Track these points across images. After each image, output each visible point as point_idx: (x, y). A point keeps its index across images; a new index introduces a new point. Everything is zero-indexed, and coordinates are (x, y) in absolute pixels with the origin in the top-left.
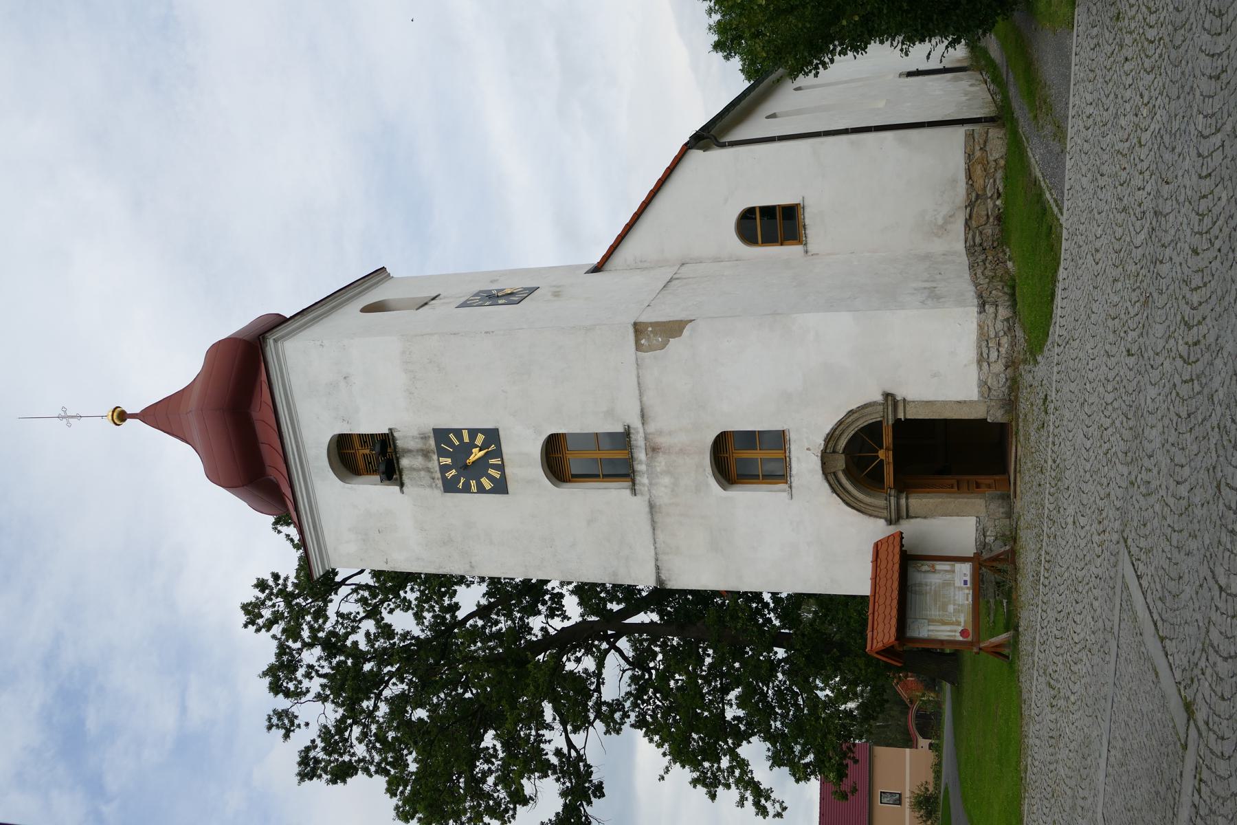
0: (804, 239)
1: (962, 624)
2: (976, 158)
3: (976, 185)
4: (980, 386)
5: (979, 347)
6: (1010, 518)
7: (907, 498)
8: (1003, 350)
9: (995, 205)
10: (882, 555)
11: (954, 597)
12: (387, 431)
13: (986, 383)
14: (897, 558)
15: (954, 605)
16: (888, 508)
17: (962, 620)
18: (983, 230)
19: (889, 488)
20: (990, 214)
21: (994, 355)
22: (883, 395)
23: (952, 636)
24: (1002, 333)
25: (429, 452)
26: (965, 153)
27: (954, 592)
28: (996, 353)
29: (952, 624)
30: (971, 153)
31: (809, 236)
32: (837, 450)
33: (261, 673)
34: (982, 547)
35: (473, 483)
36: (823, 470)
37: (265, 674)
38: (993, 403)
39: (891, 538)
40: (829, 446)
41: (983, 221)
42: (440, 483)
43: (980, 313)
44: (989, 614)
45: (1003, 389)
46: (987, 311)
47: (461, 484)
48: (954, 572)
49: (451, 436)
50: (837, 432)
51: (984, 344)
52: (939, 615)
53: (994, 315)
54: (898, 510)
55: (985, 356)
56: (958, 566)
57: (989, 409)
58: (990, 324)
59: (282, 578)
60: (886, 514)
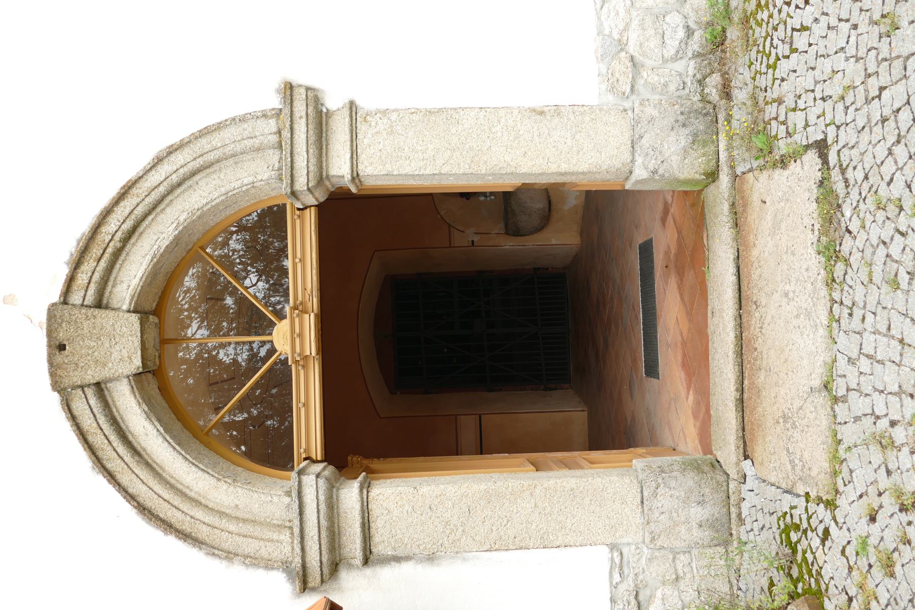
6: (726, 543)
7: (366, 487)
13: (622, 46)
32: (115, 303)
36: (52, 375)
40: (82, 278)
60: (287, 549)
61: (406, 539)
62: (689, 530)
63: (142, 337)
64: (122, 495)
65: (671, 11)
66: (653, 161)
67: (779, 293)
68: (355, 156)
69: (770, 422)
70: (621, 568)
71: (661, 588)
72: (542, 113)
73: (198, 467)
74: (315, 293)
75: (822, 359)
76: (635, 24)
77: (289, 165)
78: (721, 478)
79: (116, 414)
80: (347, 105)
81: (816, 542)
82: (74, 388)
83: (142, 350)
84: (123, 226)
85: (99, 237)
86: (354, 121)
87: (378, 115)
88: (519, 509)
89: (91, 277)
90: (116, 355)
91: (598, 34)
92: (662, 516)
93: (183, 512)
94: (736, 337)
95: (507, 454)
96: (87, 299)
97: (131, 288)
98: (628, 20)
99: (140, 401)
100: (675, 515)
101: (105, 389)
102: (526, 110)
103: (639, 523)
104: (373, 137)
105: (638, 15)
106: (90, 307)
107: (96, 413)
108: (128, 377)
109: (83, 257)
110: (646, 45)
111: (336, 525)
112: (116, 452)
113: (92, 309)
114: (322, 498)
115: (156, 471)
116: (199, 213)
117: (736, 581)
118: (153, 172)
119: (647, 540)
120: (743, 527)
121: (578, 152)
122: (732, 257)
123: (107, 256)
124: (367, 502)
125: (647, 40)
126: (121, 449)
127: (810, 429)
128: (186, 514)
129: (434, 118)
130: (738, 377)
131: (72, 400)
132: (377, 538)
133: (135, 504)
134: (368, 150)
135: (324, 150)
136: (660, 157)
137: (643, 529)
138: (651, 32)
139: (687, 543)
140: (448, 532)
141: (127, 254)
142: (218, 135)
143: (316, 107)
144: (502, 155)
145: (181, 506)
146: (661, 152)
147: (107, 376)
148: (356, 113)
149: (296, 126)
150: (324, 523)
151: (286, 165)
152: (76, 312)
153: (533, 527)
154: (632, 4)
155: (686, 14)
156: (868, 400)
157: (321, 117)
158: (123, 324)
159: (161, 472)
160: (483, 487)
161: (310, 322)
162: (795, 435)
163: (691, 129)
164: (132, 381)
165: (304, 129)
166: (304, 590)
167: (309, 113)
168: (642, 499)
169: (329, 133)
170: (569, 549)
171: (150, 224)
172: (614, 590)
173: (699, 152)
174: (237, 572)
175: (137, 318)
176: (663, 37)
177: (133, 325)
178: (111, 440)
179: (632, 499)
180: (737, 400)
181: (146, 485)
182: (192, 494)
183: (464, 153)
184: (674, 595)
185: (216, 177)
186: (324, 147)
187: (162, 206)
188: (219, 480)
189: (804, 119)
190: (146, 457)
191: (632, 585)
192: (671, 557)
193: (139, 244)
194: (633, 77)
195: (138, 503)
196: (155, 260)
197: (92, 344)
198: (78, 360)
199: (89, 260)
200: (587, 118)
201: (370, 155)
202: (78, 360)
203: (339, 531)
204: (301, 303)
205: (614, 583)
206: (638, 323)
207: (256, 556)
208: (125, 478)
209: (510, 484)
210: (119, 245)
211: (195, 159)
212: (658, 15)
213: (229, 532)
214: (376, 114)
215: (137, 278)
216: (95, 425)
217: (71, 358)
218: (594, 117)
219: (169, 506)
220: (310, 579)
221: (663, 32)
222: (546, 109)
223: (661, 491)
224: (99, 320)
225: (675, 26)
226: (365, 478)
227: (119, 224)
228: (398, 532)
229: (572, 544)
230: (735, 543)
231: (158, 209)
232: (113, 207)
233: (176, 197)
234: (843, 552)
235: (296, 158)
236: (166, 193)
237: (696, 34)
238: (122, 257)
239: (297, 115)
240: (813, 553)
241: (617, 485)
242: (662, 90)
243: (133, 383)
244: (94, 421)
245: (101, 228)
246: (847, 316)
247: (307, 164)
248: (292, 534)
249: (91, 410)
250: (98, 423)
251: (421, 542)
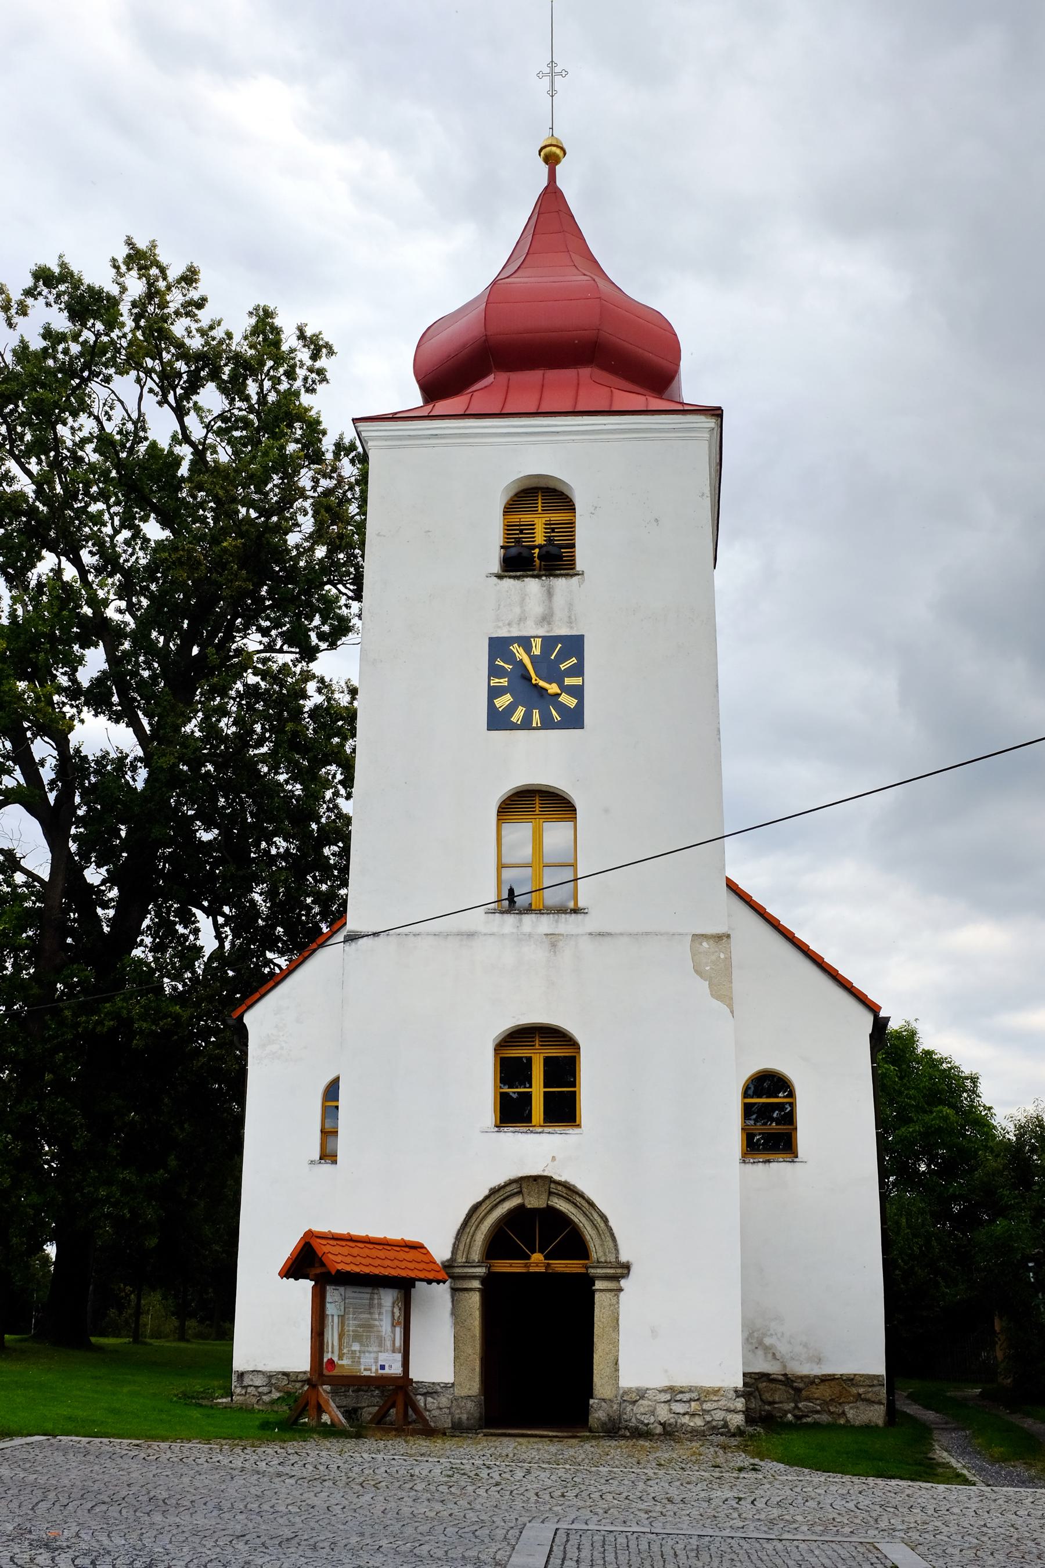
0: (752, 1161)
1: (340, 1362)
2: (848, 1388)
3: (813, 1389)
5: (691, 1390)
8: (686, 1420)
9: (786, 1412)
10: (412, 1254)
11: (368, 1352)
12: (579, 567)
13: (642, 1397)
14: (412, 1274)
15: (360, 1352)
16: (469, 1263)
17: (345, 1362)
18: (755, 1397)
19: (490, 1266)
20: (776, 1406)
21: (679, 1408)
22: (628, 1262)
23: (328, 1348)
24: (708, 1418)
25: (549, 623)
26: (855, 1375)
27: (375, 1352)
28: (682, 1411)
29: (340, 1349)
30: (854, 1382)
31: (755, 1166)
33: (66, 261)
35: (504, 682)
37: (63, 265)
40: (560, 1188)
41: (767, 1396)
42: (503, 633)
43: (736, 1391)
45: (633, 1420)
46: (737, 1400)
47: (502, 664)
48: (394, 1352)
49: (574, 660)
50: (578, 1199)
51: (694, 1395)
52: (348, 1331)
53: (733, 1408)
55: (679, 1397)
56: (399, 1357)
57: (608, 1402)
58: (720, 1403)
59: (196, 311)
60: (460, 1260)
76: (650, 1403)
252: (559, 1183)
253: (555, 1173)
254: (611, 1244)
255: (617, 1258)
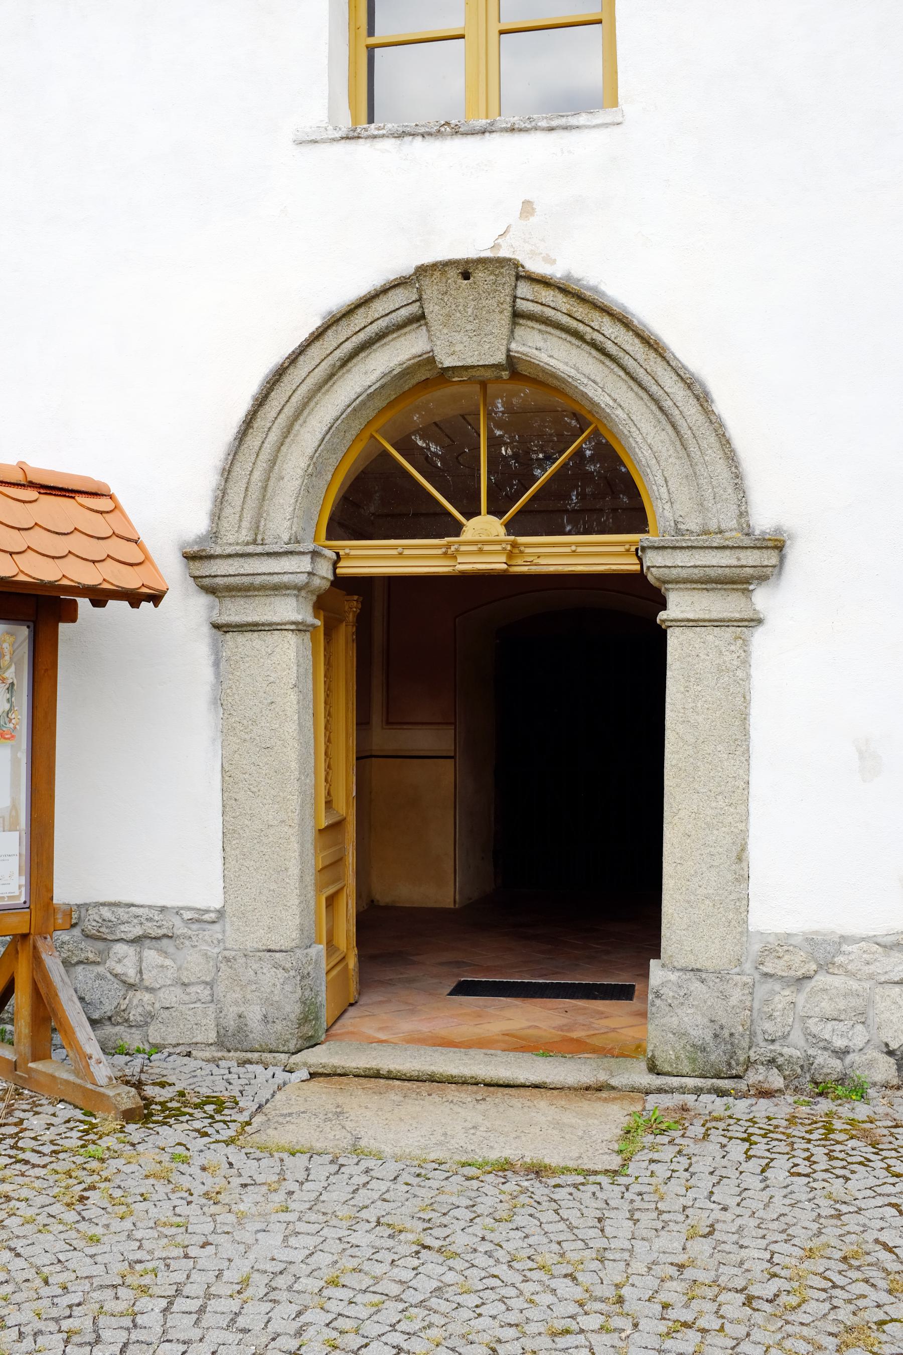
4: (811, 940)
6: (220, 1044)
7: (299, 628)
13: (826, 966)
32: (519, 332)
34: (90, 926)
36: (434, 266)
38: (736, 996)
39: (135, 555)
40: (547, 295)
44: (533, 327)
45: (797, 1037)
54: (263, 588)
60: (231, 539)
61: (238, 674)
62: (236, 1003)
63: (478, 366)
64: (296, 349)
65: (869, 1032)
66: (671, 994)
67: (481, 1121)
68: (691, 624)
69: (340, 1100)
70: (198, 921)
71: (175, 966)
72: (740, 859)
73: (327, 433)
74: (534, 569)
75: (387, 1149)
76: (854, 985)
77: (677, 545)
78: (292, 1047)
79: (390, 337)
80: (755, 616)
81: (197, 1125)
82: (420, 291)
83: (462, 367)
84: (610, 342)
85: (597, 314)
86: (735, 624)
87: (743, 654)
88: (267, 806)
89: (549, 306)
90: (458, 337)
91: (842, 937)
92: (252, 973)
93: (276, 418)
94: (452, 1076)
95: (354, 794)
96: (522, 301)
97: (536, 352)
98: (859, 976)
99: (404, 366)
100: (254, 987)
101: (419, 324)
102: (744, 839)
103: (246, 945)
104: (716, 647)
105: (864, 989)
106: (514, 306)
107: (390, 316)
108: (432, 351)
109: (573, 297)
110: (825, 997)
111: (256, 593)
112: (346, 341)
113: (510, 309)
114: (285, 579)
115: (324, 385)
116: (627, 433)
117: (178, 1052)
118: (675, 378)
119: (227, 953)
120: (236, 1064)
121: (688, 902)
122: (548, 1081)
123: (574, 324)
124: (281, 630)
125: (831, 999)
126: (349, 346)
127: (317, 1133)
128: (274, 422)
129: (737, 723)
130: (405, 1075)
131: (405, 289)
132: (241, 639)
133: (286, 365)
134: (699, 640)
135: (699, 586)
136: (676, 1002)
137: (240, 949)
138: (842, 1004)
139: (222, 999)
140: (245, 722)
141: (578, 347)
142: (719, 457)
143: (753, 577)
144: (687, 807)
145: (282, 416)
146: (682, 1004)
147: (432, 328)
148: (746, 626)
149: (727, 552)
150: (258, 580)
151: (677, 541)
152: (507, 291)
153: (247, 822)
154: (880, 983)
155: (865, 1051)
156: (323, 1178)
157: (742, 583)
158: (493, 345)
159: (323, 390)
160: (294, 765)
161: (495, 563)
162: (317, 1120)
163: (711, 1045)
164: (427, 356)
165: (724, 562)
166: (185, 557)
167: (744, 569)
168: (273, 951)
169: (723, 592)
170: (221, 861)
171: (615, 373)
172: (175, 911)
173: (682, 1052)
174: (208, 480)
175: (500, 360)
176: (835, 1020)
177: (492, 356)
178: (359, 334)
179: (273, 939)
180: (378, 1070)
181: (308, 375)
182: (297, 427)
183: (692, 760)
184: (167, 980)
185: (671, 452)
186: (704, 586)
187: (636, 387)
188: (312, 458)
189: (660, 1159)
190: (340, 374)
191: (179, 932)
192: (208, 979)
193: (591, 360)
194: (783, 977)
195: (287, 367)
196: (570, 380)
197: (470, 311)
198: (451, 295)
199: (569, 304)
200: (731, 916)
201: (692, 643)
202: (451, 295)
203: (250, 596)
204: (521, 552)
205: (182, 912)
206: (533, 977)
207: (224, 503)
208: (316, 352)
209: (296, 797)
210: (588, 337)
211: (690, 428)
212: (865, 1015)
213: (251, 472)
214: (745, 651)
215: (549, 359)
216: (376, 316)
217: (453, 286)
218: (732, 924)
219: (283, 403)
220: (197, 564)
221: (841, 1021)
222: (744, 865)
223: (281, 973)
224: (497, 316)
225: (849, 1036)
226: (314, 627)
227: (613, 338)
228: (247, 665)
229: (227, 865)
230: (220, 1054)
231: (632, 383)
232: (633, 330)
233: (646, 405)
234: (180, 1144)
235: (687, 553)
236: (650, 393)
237: (838, 1061)
238: (573, 340)
239: (742, 554)
240: (187, 1121)
241: (290, 923)
242: (765, 1013)
243: (425, 356)
244: (381, 315)
245: (607, 317)
246: (418, 1172)
247: (679, 567)
248: (247, 544)
249: (394, 311)
250: (378, 319)
251: (234, 690)
252: (544, 282)
253: (533, 253)
254: (721, 468)
255: (743, 514)
